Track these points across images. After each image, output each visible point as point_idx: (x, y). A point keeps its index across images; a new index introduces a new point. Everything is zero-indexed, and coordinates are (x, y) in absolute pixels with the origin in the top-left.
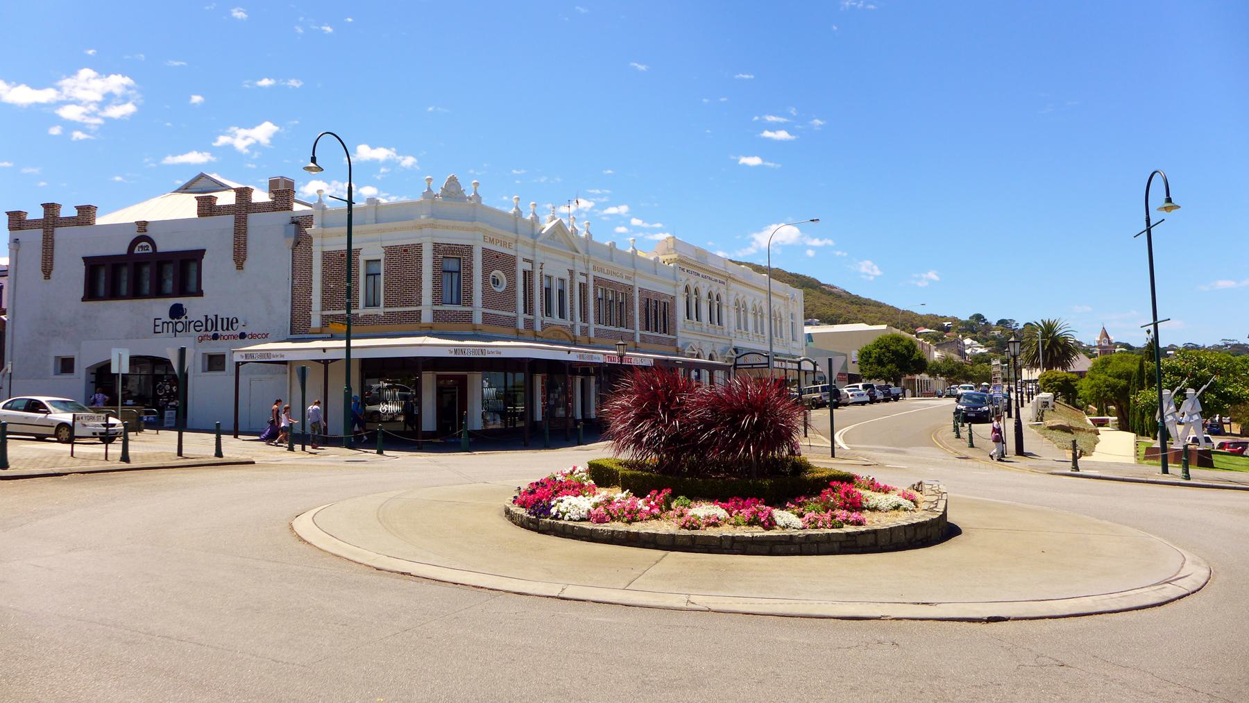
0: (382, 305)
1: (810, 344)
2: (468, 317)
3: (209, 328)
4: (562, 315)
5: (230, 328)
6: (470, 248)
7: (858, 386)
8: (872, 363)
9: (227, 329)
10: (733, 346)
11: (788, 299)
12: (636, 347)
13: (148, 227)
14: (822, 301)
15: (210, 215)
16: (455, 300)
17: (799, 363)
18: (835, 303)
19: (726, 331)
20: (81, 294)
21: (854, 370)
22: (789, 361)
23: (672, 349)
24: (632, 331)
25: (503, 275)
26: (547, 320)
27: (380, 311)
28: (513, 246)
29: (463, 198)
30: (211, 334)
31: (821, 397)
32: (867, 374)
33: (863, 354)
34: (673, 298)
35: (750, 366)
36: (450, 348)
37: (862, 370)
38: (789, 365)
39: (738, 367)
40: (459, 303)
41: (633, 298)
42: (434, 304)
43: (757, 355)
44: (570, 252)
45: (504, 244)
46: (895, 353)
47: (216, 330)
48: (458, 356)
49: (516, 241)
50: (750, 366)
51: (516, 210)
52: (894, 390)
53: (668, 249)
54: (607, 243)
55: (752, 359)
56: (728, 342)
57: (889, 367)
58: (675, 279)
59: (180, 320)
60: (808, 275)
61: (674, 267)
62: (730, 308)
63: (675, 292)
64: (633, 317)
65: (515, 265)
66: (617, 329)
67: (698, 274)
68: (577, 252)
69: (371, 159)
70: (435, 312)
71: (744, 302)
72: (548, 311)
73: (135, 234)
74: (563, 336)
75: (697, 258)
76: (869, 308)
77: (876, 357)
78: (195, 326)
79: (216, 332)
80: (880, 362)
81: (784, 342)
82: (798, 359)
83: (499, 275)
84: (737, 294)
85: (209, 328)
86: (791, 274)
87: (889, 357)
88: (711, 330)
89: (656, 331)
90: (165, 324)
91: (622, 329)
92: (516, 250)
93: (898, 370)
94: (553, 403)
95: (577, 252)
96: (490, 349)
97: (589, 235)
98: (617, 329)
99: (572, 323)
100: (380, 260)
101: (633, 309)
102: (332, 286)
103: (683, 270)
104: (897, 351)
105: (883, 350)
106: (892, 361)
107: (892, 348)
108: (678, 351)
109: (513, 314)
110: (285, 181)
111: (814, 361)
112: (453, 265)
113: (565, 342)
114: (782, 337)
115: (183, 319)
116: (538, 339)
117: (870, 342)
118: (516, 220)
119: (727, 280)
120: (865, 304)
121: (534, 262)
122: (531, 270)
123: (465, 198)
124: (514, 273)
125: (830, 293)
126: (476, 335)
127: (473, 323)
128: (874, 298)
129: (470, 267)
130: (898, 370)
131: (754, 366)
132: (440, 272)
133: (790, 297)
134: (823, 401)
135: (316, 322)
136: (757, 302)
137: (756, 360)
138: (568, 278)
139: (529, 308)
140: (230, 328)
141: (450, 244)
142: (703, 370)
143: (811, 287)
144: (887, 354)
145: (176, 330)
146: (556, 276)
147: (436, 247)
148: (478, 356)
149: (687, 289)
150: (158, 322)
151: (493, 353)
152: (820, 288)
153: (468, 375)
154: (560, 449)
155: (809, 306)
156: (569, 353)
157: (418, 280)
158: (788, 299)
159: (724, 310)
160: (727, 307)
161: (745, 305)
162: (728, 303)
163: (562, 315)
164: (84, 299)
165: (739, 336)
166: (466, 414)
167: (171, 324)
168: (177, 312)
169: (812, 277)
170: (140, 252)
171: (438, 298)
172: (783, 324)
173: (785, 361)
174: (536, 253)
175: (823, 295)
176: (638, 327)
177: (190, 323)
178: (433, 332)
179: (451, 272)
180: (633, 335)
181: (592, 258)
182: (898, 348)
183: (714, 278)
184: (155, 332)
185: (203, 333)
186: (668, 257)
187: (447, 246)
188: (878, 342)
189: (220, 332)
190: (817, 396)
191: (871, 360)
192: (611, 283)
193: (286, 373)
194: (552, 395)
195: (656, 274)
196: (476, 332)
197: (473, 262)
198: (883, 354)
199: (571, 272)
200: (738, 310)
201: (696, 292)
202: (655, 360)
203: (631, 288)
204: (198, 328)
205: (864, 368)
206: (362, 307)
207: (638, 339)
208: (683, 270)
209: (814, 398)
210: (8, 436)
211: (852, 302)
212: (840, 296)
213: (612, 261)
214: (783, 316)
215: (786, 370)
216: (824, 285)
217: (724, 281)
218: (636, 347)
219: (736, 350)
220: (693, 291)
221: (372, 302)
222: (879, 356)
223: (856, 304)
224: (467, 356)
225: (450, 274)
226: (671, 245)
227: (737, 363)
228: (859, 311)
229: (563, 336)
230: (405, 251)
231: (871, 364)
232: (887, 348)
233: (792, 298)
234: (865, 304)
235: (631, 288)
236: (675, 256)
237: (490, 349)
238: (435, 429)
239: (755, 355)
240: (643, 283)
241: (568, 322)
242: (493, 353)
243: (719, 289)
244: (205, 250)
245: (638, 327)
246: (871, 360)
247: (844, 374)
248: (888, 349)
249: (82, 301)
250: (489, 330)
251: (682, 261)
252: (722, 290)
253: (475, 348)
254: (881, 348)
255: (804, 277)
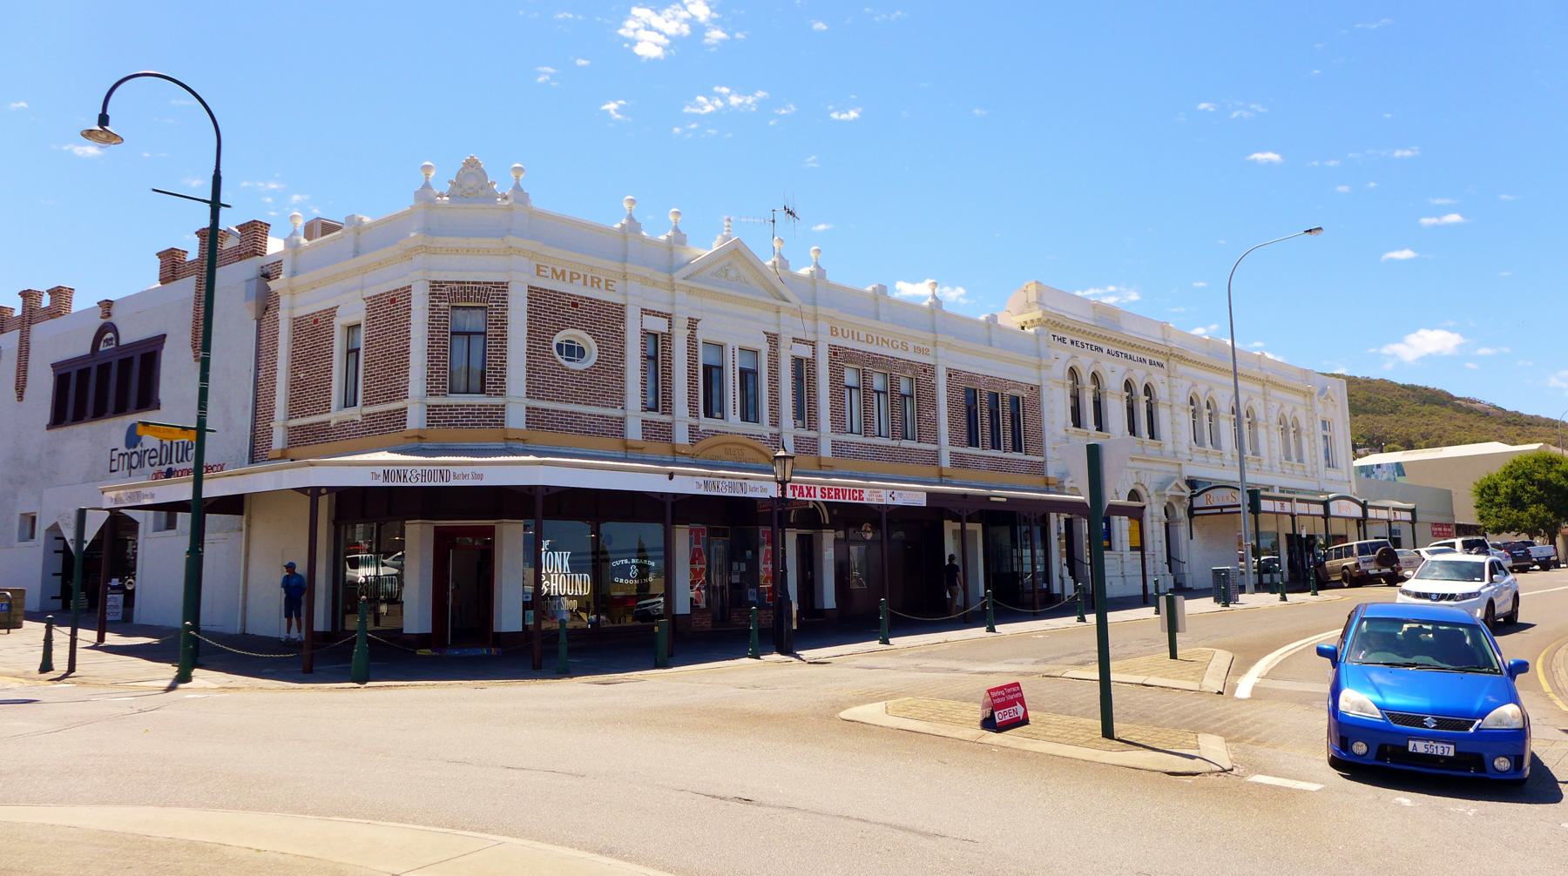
0: (360, 403)
1: (1401, 480)
2: (495, 417)
3: (164, 461)
4: (749, 411)
5: (185, 459)
6: (502, 288)
7: (1453, 545)
8: (1501, 504)
9: (182, 460)
10: (1185, 476)
11: (1312, 394)
12: (941, 476)
13: (115, 310)
14: (1457, 423)
15: (175, 280)
16: (476, 383)
17: (1326, 504)
18: (1479, 424)
19: (1266, 462)
20: (47, 419)
21: (1467, 513)
22: (1299, 501)
23: (1038, 481)
24: (934, 447)
25: (589, 338)
26: (705, 423)
27: (355, 414)
28: (618, 284)
29: (492, 196)
30: (164, 468)
31: (1357, 565)
32: (1493, 523)
33: (1483, 490)
34: (1036, 389)
35: (1219, 511)
36: (373, 469)
37: (1482, 517)
38: (1301, 508)
39: (1196, 512)
40: (482, 391)
41: (933, 387)
42: (430, 393)
43: (1231, 490)
44: (772, 301)
45: (595, 282)
46: (1544, 485)
47: (171, 463)
48: (390, 484)
49: (935, 344)
50: (1219, 511)
51: (933, 300)
52: (1540, 547)
53: (1028, 304)
54: (982, 318)
55: (1218, 498)
56: (1175, 468)
57: (1533, 509)
58: (1039, 355)
59: (135, 450)
60: (1431, 386)
61: (1037, 334)
62: (1177, 409)
63: (1040, 379)
64: (934, 422)
65: (622, 320)
66: (895, 443)
67: (1098, 349)
68: (786, 300)
69: (914, 295)
70: (431, 409)
71: (1295, 418)
72: (712, 407)
73: (99, 322)
74: (749, 454)
75: (1096, 321)
76: (1536, 429)
77: (1507, 493)
78: (150, 458)
79: (170, 466)
80: (1515, 502)
81: (1308, 469)
82: (1323, 497)
83: (580, 338)
84: (1282, 406)
85: (164, 461)
86: (1404, 386)
87: (1533, 493)
88: (1287, 468)
89: (996, 445)
90: (121, 457)
91: (906, 444)
92: (625, 295)
93: (1551, 515)
94: (738, 581)
95: (786, 300)
96: (458, 470)
97: (820, 273)
98: (895, 443)
99: (775, 430)
100: (360, 325)
101: (934, 407)
102: (302, 375)
103: (1063, 340)
104: (1549, 481)
105: (1520, 481)
106: (1538, 500)
107: (1538, 476)
108: (1047, 484)
109: (617, 412)
110: (323, 224)
111: (1362, 501)
112: (473, 321)
113: (756, 466)
114: (1300, 460)
115: (138, 449)
116: (679, 459)
117: (1497, 470)
118: (989, 327)
119: (1168, 361)
120: (1529, 424)
121: (673, 317)
122: (810, 356)
123: (493, 196)
124: (620, 337)
125: (1470, 411)
126: (527, 450)
127: (505, 427)
128: (1544, 415)
129: (502, 323)
130: (1551, 515)
131: (1225, 510)
132: (444, 336)
133: (1316, 390)
134: (1362, 572)
135: (278, 440)
136: (1287, 410)
137: (1227, 497)
138: (764, 348)
139: (658, 398)
140: (185, 459)
141: (464, 283)
142: (1116, 518)
143: (1437, 404)
144: (1529, 488)
145: (132, 467)
146: (732, 342)
147: (436, 289)
148: (432, 484)
149: (1128, 385)
150: (115, 454)
151: (465, 476)
152: (1453, 405)
153: (496, 525)
154: (538, 681)
155: (1434, 431)
156: (671, 477)
157: (405, 351)
158: (1312, 394)
159: (1262, 432)
160: (1267, 427)
161: (1296, 422)
162: (1267, 421)
163: (749, 411)
164: (50, 427)
165: (1197, 458)
166: (1344, 587)
167: (126, 456)
168: (132, 438)
169: (1438, 388)
170: (106, 348)
171: (440, 380)
172: (1305, 439)
173: (1290, 500)
174: (819, 330)
175: (1459, 415)
176: (944, 438)
177: (145, 452)
178: (425, 445)
179: (469, 334)
180: (936, 455)
181: (939, 339)
182: (1552, 476)
183: (1136, 355)
184: (111, 471)
185: (157, 468)
186: (1027, 317)
187: (457, 286)
188: (1511, 467)
189: (175, 466)
190: (1349, 562)
191: (1498, 500)
192: (875, 360)
193: (241, 530)
194: (735, 566)
195: (991, 345)
196: (510, 443)
197: (508, 313)
198: (1522, 487)
199: (773, 339)
200: (1285, 431)
201: (1148, 390)
202: (930, 495)
203: (929, 370)
204: (152, 461)
205: (1485, 513)
206: (335, 409)
207: (946, 462)
208: (1063, 340)
209: (1346, 567)
210: (339, 629)
211: (1508, 422)
212: (1488, 414)
213: (878, 318)
214: (1303, 424)
215: (1293, 516)
216: (1459, 399)
217: (1160, 361)
218: (941, 476)
219: (1192, 483)
220: (1140, 390)
221: (350, 401)
222: (1514, 491)
223: (1516, 425)
224: (409, 484)
225: (466, 337)
226: (1033, 297)
227: (1195, 506)
228: (1518, 435)
229: (749, 454)
230: (393, 301)
231: (1499, 505)
232: (1528, 476)
233: (1320, 394)
234: (1529, 424)
235: (929, 370)
236: (1037, 314)
237: (458, 470)
238: (430, 631)
239: (1229, 489)
240: (945, 360)
241: (764, 428)
242: (465, 476)
243: (1149, 374)
244: (165, 336)
245: (944, 438)
246: (1498, 500)
247: (1448, 526)
248: (1530, 479)
249: (47, 429)
250: (441, 434)
251: (1056, 325)
252: (1158, 379)
253: (427, 468)
254: (1516, 478)
255: (1426, 389)
